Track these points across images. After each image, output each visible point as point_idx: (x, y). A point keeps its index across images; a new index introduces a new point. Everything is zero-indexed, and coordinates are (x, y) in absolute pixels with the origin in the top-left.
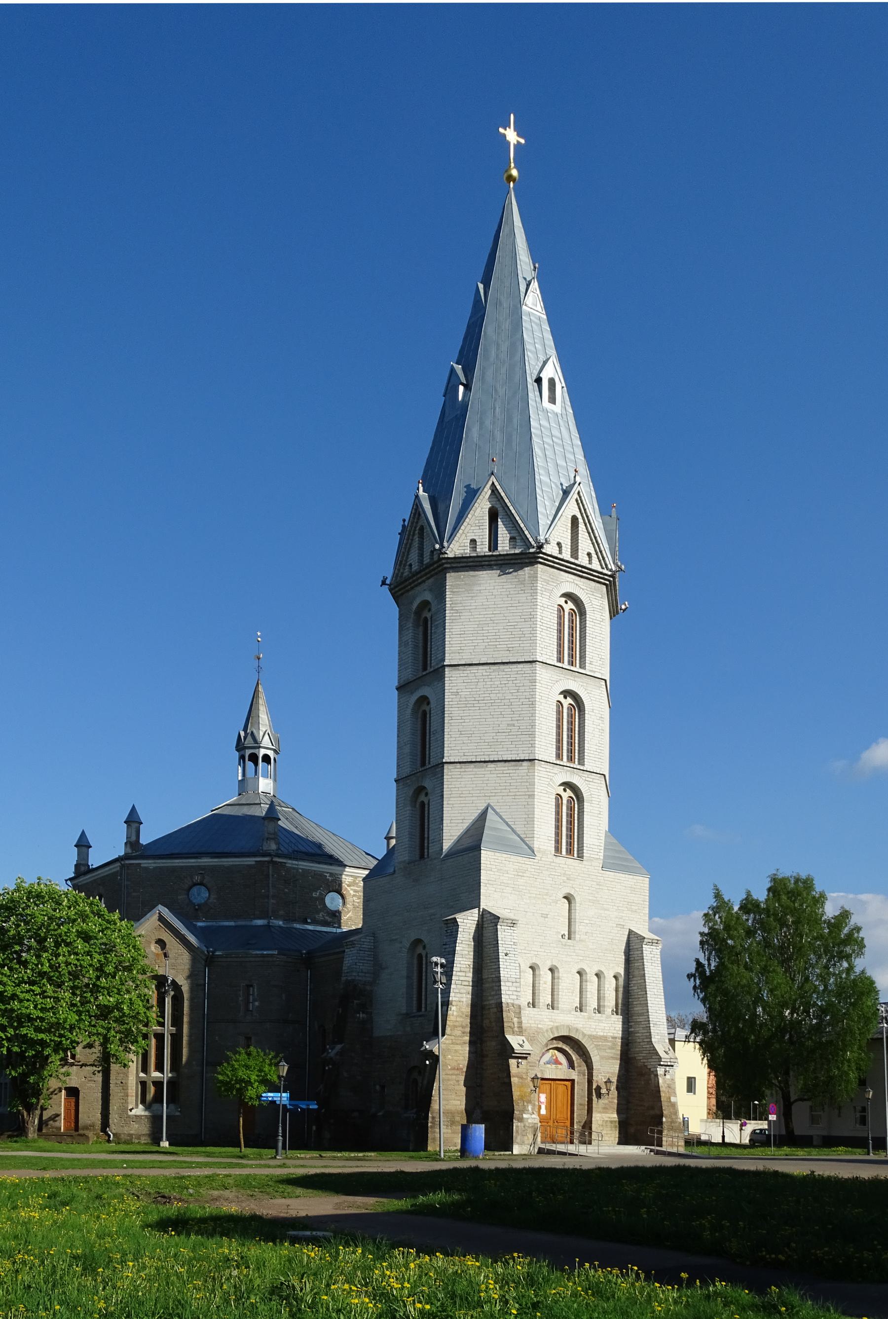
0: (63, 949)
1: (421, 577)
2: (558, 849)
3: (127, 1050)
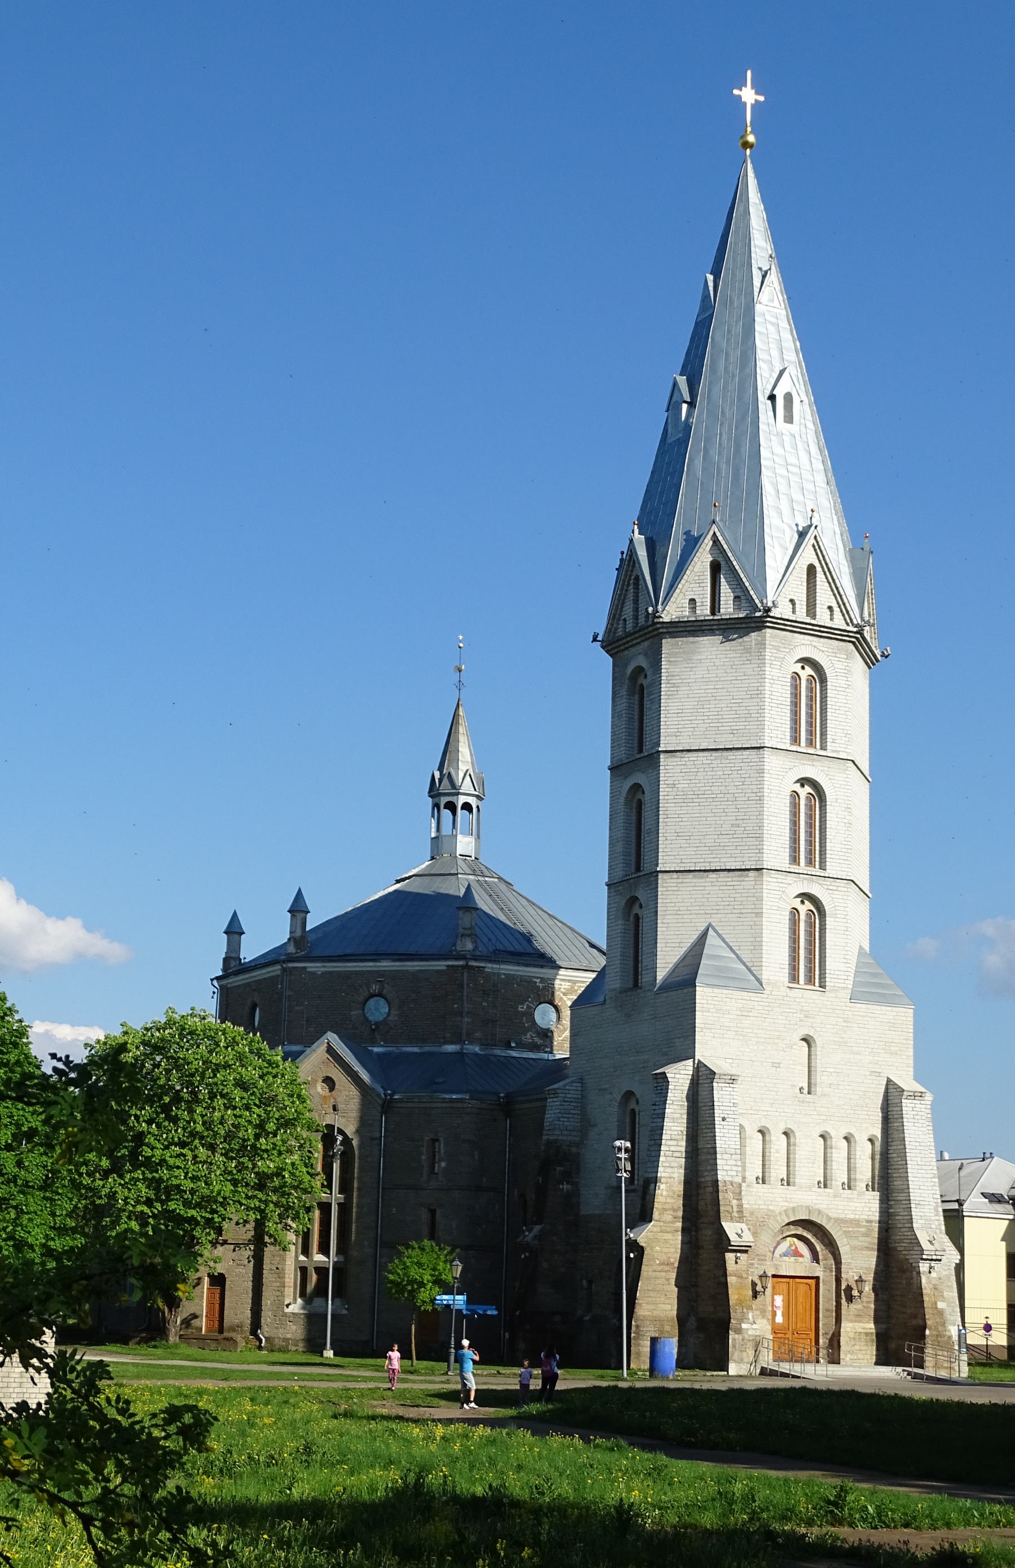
0: (219, 1102)
1: (636, 638)
2: (794, 978)
3: (287, 1228)
